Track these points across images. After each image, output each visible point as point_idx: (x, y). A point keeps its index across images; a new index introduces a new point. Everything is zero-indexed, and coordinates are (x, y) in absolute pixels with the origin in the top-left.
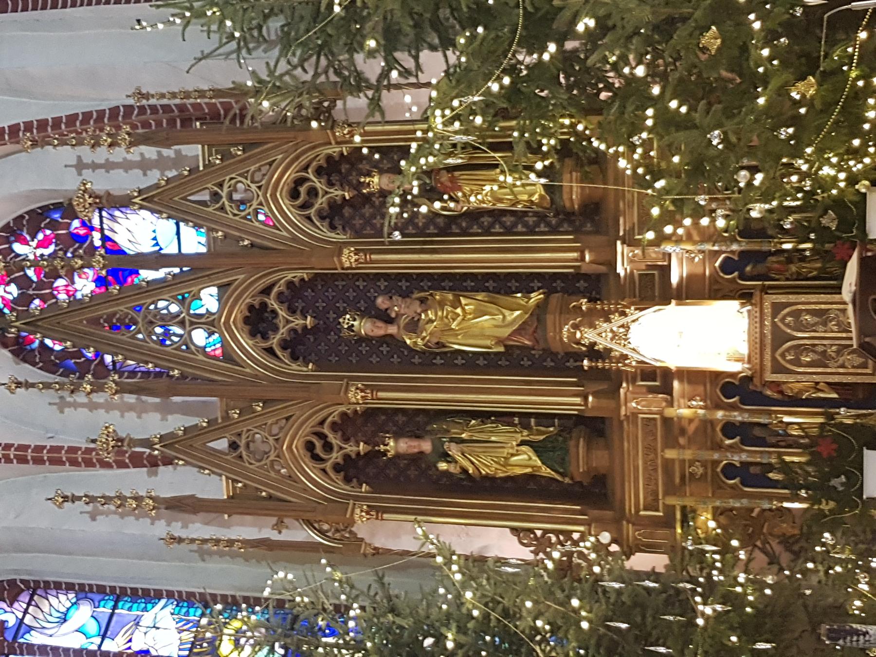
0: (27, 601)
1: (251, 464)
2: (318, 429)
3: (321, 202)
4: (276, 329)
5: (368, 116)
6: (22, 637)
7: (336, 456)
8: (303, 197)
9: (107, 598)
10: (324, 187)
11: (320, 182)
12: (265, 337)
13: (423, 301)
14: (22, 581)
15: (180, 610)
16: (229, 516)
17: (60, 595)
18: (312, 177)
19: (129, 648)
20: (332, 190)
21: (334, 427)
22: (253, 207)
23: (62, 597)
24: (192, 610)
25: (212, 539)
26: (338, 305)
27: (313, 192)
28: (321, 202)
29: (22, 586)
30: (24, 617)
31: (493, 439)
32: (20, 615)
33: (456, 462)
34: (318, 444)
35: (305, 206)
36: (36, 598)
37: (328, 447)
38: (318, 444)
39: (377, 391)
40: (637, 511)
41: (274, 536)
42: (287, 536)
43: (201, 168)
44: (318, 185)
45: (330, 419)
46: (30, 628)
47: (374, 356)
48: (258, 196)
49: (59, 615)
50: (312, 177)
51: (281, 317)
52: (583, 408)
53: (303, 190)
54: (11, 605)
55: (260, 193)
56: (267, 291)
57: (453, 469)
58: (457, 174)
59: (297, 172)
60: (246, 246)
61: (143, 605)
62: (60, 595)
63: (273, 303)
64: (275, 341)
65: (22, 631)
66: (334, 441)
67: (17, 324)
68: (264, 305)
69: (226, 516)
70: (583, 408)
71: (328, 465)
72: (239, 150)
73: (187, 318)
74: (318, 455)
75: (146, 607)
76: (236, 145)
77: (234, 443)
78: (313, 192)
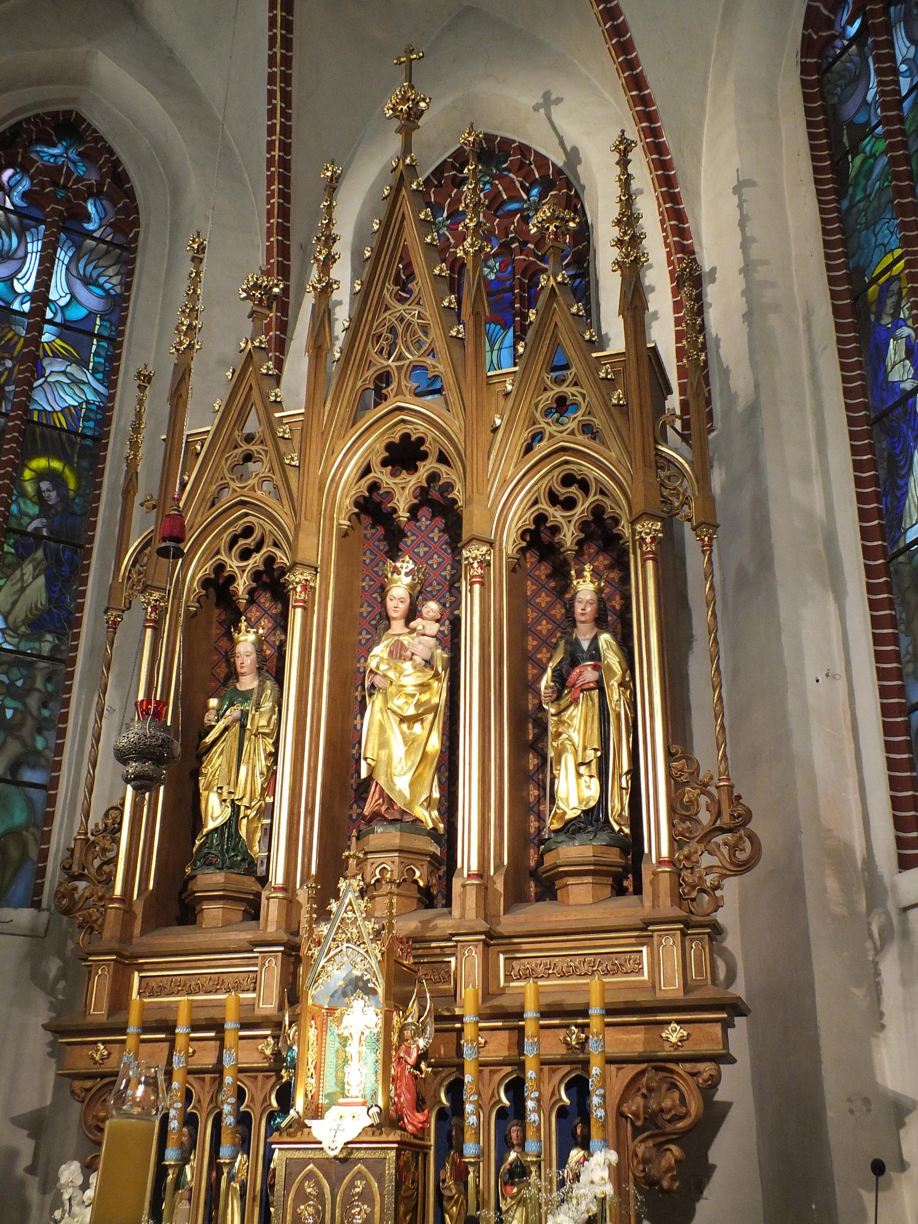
0: (115, 242)
1: (227, 459)
2: (268, 540)
3: (556, 515)
4: (394, 475)
5: (429, 386)
6: (68, 238)
7: (233, 564)
8: (563, 492)
9: (113, 328)
10: (576, 518)
11: (583, 512)
12: (384, 463)
13: (429, 663)
14: (137, 233)
15: (92, 410)
16: (164, 440)
17: (119, 277)
18: (591, 499)
19: (46, 355)
20: (572, 528)
21: (270, 560)
22: (546, 426)
23: (115, 280)
24: (91, 424)
25: (140, 424)
26: (435, 556)
27: (569, 504)
28: (556, 515)
29: (131, 236)
30: (95, 239)
31: (243, 769)
32: (96, 235)
33: (218, 721)
34: (250, 542)
35: (553, 499)
36: (118, 251)
37: (245, 555)
38: (250, 542)
39: (304, 608)
40: (140, 968)
41: (138, 498)
42: (137, 512)
43: (594, 355)
44: (579, 510)
45: (279, 553)
46: (78, 247)
47: (370, 609)
48: (561, 432)
49: (95, 275)
50: (591, 499)
51: (409, 479)
52: (654, 861)
53: (574, 490)
54: (111, 225)
55: (564, 434)
56: (443, 459)
57: (210, 717)
58: (596, 693)
59: (595, 479)
60: (494, 422)
61: (101, 369)
62: (119, 277)
63: (425, 468)
64: (379, 475)
65: (76, 238)
66: (251, 561)
67: (401, 167)
68: (424, 456)
69: (164, 437)
70: (654, 861)
71: (223, 557)
72: (619, 399)
73: (407, 362)
74: (237, 542)
75: (99, 372)
76: (626, 395)
77: (253, 438)
78: (569, 504)
